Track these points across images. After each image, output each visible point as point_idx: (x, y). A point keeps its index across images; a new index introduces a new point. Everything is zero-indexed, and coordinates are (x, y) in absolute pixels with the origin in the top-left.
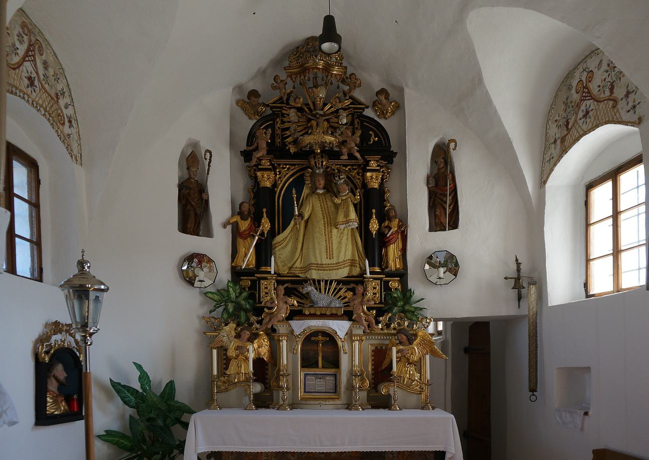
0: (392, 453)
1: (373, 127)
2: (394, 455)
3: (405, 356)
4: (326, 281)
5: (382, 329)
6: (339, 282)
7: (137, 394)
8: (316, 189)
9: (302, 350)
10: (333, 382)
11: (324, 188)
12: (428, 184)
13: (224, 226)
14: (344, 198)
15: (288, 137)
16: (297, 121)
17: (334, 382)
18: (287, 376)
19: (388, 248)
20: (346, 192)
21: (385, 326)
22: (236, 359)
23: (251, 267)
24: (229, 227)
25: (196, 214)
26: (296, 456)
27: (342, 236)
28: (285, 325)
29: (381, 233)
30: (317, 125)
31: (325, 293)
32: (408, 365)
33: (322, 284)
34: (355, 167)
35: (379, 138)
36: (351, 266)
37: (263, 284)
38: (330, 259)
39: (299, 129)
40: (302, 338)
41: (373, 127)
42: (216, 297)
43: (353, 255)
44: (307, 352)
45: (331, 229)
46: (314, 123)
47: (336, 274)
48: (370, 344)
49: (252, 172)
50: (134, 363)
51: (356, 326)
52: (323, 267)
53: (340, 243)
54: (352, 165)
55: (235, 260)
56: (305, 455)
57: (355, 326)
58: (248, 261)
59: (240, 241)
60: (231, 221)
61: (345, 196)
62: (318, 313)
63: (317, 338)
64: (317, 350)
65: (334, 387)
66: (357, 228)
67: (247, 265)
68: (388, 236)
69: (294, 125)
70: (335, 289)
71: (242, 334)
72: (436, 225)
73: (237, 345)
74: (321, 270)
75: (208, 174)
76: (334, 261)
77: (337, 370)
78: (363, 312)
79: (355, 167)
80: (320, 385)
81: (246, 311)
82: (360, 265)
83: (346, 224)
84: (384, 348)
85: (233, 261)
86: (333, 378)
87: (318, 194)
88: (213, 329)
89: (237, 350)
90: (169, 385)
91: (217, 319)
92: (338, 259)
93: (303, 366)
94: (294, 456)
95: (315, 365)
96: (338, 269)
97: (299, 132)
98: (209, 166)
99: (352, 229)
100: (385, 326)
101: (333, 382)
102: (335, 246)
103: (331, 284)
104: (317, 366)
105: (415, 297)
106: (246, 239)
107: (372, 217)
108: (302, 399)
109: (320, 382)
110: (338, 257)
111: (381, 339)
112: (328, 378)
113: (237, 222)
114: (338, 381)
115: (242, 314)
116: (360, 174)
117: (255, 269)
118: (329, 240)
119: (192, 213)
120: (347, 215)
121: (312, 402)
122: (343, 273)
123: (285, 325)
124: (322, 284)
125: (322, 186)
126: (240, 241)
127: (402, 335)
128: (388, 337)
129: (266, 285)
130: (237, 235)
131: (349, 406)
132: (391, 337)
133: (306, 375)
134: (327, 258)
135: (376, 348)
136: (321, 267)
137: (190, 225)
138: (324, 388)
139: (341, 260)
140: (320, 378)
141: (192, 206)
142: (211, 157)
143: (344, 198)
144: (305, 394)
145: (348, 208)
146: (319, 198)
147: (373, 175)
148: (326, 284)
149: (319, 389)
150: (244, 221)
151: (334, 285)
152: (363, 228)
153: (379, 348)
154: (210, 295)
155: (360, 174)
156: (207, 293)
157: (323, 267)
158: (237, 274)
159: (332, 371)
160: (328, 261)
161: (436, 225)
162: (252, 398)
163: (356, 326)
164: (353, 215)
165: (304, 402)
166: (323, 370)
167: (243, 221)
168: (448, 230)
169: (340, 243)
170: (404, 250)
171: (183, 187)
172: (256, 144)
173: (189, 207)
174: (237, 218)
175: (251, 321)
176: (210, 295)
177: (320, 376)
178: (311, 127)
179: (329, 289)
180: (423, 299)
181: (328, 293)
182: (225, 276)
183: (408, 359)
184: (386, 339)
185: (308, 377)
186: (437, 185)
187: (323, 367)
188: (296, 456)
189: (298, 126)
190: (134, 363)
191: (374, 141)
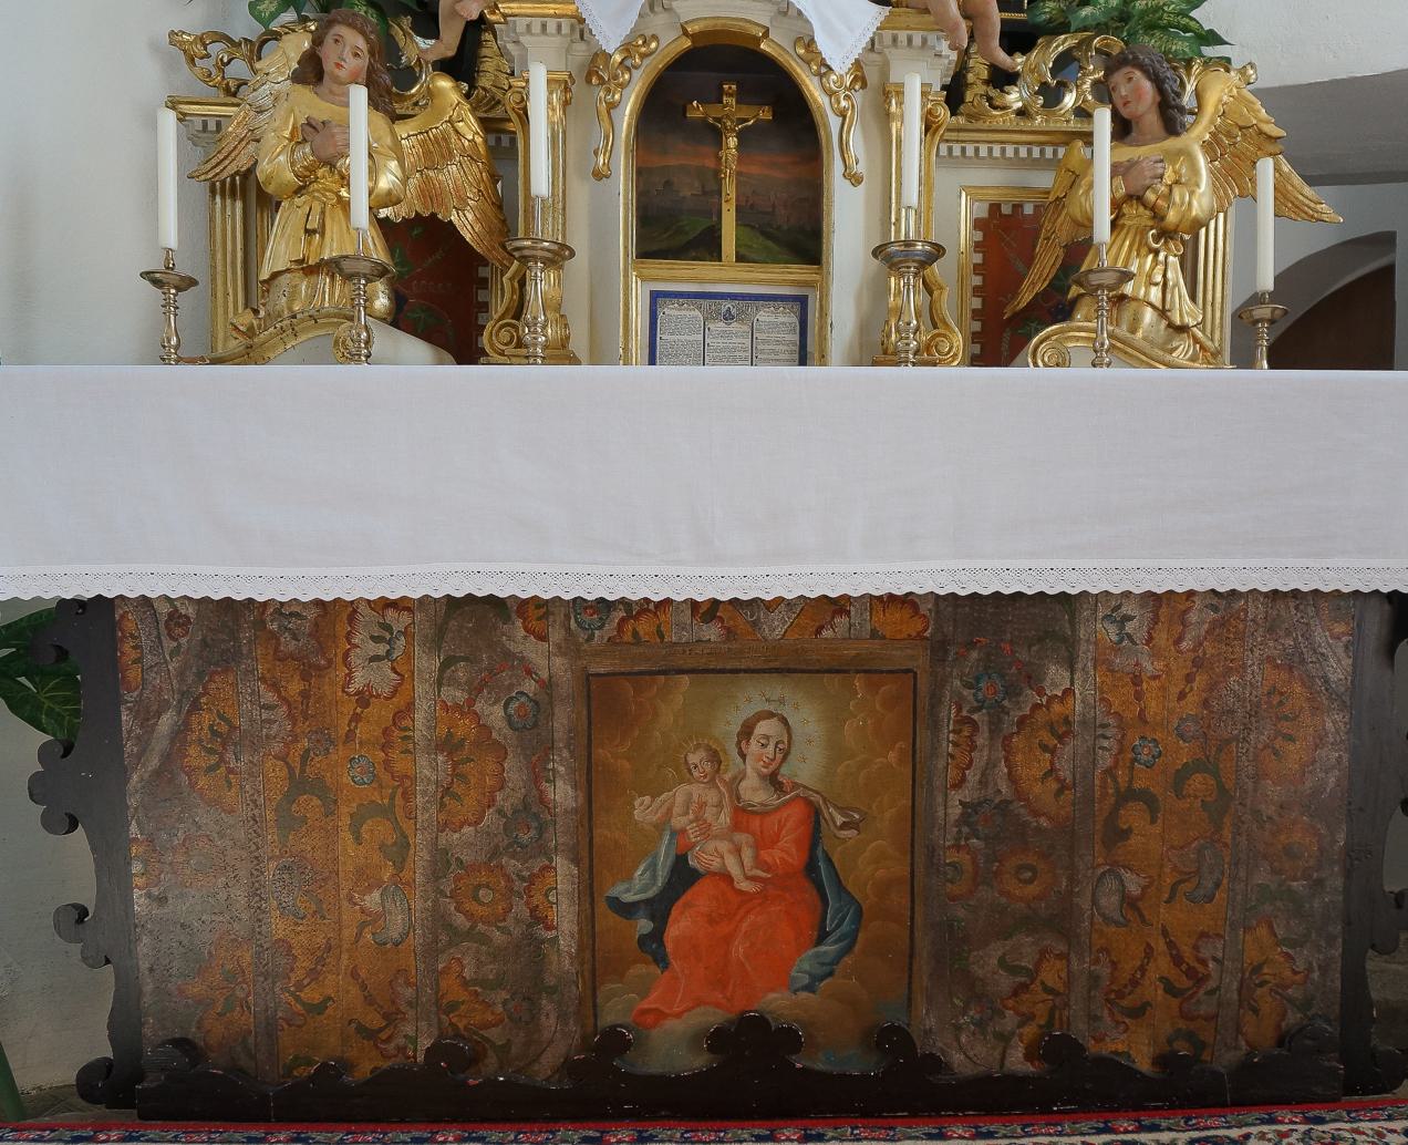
2: (1129, 627)
3: (1140, 199)
5: (1021, 113)
10: (789, 337)
17: (796, 338)
21: (1037, 93)
22: (299, 191)
32: (1157, 239)
44: (668, 184)
48: (964, 188)
51: (910, 40)
57: (902, 36)
63: (714, 112)
64: (717, 173)
71: (329, 54)
77: (800, 272)
84: (1029, 210)
86: (787, 318)
95: (706, 246)
100: (1037, 93)
101: (789, 337)
109: (728, 335)
111: (1017, 163)
112: (765, 316)
114: (812, 329)
127: (1138, 74)
128: (1049, 151)
132: (1061, 151)
133: (656, 297)
135: (995, 208)
140: (728, 317)
153: (1006, 210)
159: (779, 278)
163: (910, 40)
166: (743, 271)
177: (727, 305)
183: (1157, 216)
185: (669, 311)
187: (740, 258)
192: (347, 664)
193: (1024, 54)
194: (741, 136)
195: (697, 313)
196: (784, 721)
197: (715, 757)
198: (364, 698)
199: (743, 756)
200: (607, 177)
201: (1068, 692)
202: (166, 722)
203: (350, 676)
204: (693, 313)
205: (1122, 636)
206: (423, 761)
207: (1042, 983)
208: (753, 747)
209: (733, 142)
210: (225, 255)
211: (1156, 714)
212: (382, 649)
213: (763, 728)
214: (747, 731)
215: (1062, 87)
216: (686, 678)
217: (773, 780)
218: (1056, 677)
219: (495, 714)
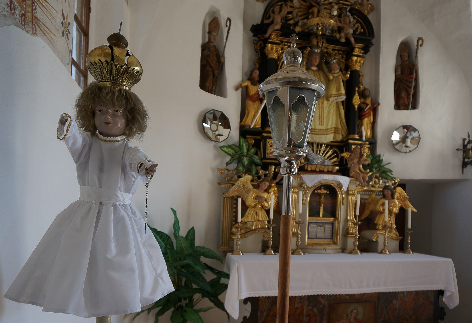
0: (403, 293)
1: (361, 21)
4: (318, 144)
6: (327, 146)
7: (168, 240)
8: (312, 65)
9: (310, 201)
11: (317, 66)
12: (396, 71)
13: (237, 89)
14: (336, 75)
15: (290, 20)
16: (298, 7)
18: (302, 223)
19: (363, 120)
20: (337, 72)
23: (257, 127)
24: (240, 91)
25: (214, 75)
26: (326, 298)
27: (330, 107)
28: (296, 179)
29: (361, 109)
30: (319, 12)
31: (317, 153)
33: (315, 146)
34: (340, 52)
35: (364, 30)
36: (335, 133)
37: (268, 142)
38: (322, 125)
39: (300, 14)
40: (312, 190)
41: (361, 21)
42: (231, 151)
43: (337, 124)
45: (323, 100)
46: (315, 10)
47: (326, 139)
49: (258, 45)
50: (171, 208)
51: (353, 182)
52: (316, 132)
53: (329, 112)
54: (338, 50)
55: (244, 120)
56: (333, 297)
58: (256, 121)
59: (249, 103)
60: (243, 85)
61: (336, 73)
62: (326, 170)
65: (331, 234)
66: (342, 102)
67: (255, 125)
68: (366, 110)
69: (297, 10)
70: (324, 151)
72: (400, 104)
73: (255, 195)
74: (314, 134)
75: (227, 40)
76: (324, 127)
78: (360, 170)
79: (340, 52)
80: (320, 232)
81: (257, 165)
82: (341, 132)
83: (338, 96)
85: (241, 121)
86: (330, 226)
87: (313, 70)
88: (227, 179)
89: (256, 199)
90: (192, 231)
91: (230, 171)
92: (327, 125)
93: (310, 216)
94: (324, 298)
96: (327, 134)
97: (300, 16)
98: (228, 33)
99: (337, 103)
102: (325, 115)
103: (321, 147)
104: (319, 216)
105: (384, 162)
106: (255, 102)
107: (354, 94)
108: (308, 244)
110: (327, 125)
112: (327, 226)
113: (247, 87)
115: (254, 167)
116: (344, 59)
117: (261, 129)
118: (321, 109)
119: (211, 73)
120: (338, 89)
121: (318, 247)
122: (329, 138)
123: (296, 179)
124: (315, 146)
125: (316, 64)
126: (249, 103)
128: (367, 193)
129: (271, 143)
130: (246, 97)
131: (343, 250)
132: (369, 193)
134: (319, 124)
136: (314, 132)
137: (208, 84)
138: (323, 235)
139: (329, 127)
140: (321, 226)
141: (211, 66)
142: (230, 25)
143: (336, 75)
144: (309, 240)
145: (339, 83)
146: (314, 74)
147: (357, 59)
148: (317, 147)
149: (319, 235)
150: (254, 86)
151: (323, 146)
152: (348, 104)
154: (225, 149)
155: (344, 59)
156: (223, 147)
157: (316, 132)
158: (244, 132)
160: (321, 127)
161: (400, 104)
162: (271, 244)
164: (343, 91)
165: (310, 247)
167: (253, 86)
168: (411, 109)
169: (329, 112)
170: (374, 123)
171: (204, 47)
172: (271, 19)
173: (208, 68)
174: (247, 83)
175: (259, 175)
176: (225, 149)
178: (313, 13)
179: (320, 151)
180: (390, 163)
181: (324, 156)
182: (234, 133)
184: (366, 194)
185: (311, 225)
186: (402, 72)
187: (323, 216)
188: (326, 298)
189: (300, 12)
190: (171, 208)
191: (360, 32)
192: (294, 303)
193: (396, 228)
194: (324, 196)
195: (316, 226)
196: (357, 310)
197: (347, 316)
198: (296, 309)
199: (351, 315)
200: (304, 204)
201: (397, 304)
202: (265, 314)
203: (295, 306)
204: (315, 226)
205: (404, 295)
206: (305, 318)
207: (212, 308)
208: (353, 314)
209: (323, 197)
210: (226, 209)
211: (267, 191)
212: (300, 301)
213: (354, 311)
214: (352, 311)
215: (369, 182)
216: (344, 304)
217: (355, 319)
218: (395, 302)
219: (316, 310)
